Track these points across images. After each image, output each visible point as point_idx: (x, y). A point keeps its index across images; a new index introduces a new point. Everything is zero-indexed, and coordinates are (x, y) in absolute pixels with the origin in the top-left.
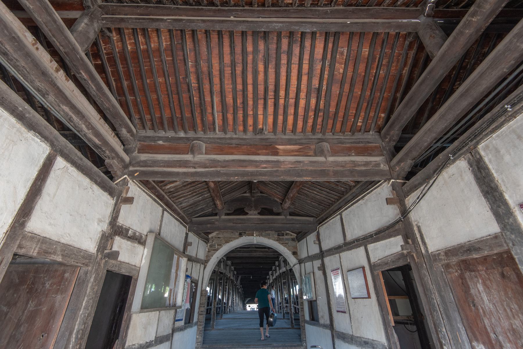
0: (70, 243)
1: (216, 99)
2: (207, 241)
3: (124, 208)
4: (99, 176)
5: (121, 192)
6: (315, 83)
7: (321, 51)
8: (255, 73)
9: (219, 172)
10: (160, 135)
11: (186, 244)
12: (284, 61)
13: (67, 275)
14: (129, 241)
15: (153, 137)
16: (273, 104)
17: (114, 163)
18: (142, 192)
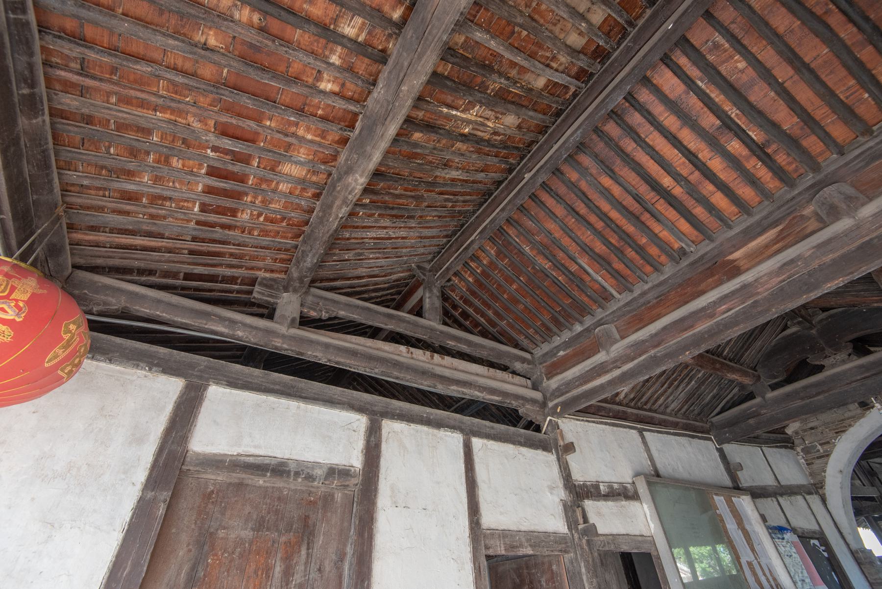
0: (532, 528)
1: (584, 262)
2: (787, 443)
3: (571, 459)
4: (520, 435)
5: (556, 440)
6: (710, 121)
7: (675, 81)
8: (606, 193)
9: (655, 356)
10: (556, 344)
11: (732, 469)
12: (629, 146)
13: (554, 567)
14: (609, 500)
15: (551, 351)
16: (666, 205)
17: (527, 409)
18: (586, 423)
